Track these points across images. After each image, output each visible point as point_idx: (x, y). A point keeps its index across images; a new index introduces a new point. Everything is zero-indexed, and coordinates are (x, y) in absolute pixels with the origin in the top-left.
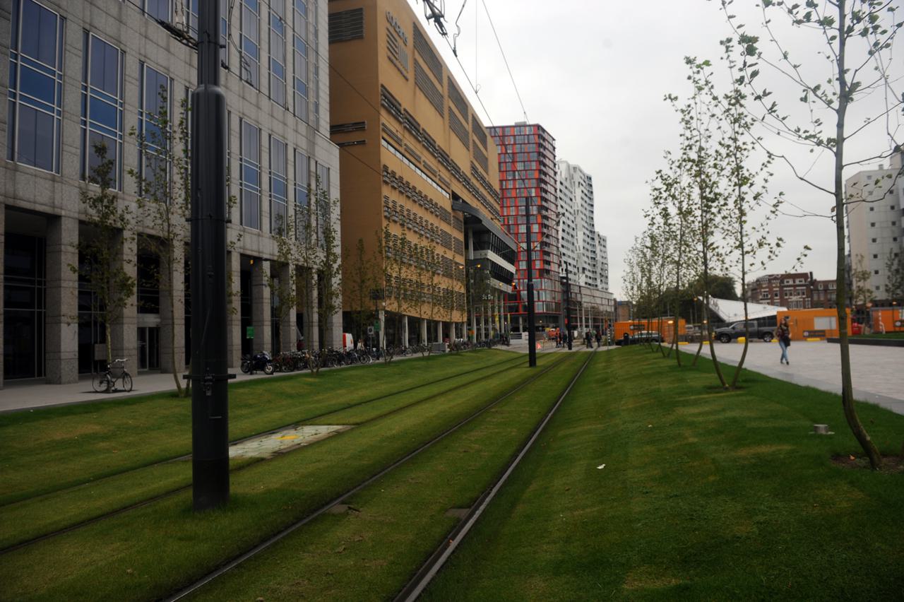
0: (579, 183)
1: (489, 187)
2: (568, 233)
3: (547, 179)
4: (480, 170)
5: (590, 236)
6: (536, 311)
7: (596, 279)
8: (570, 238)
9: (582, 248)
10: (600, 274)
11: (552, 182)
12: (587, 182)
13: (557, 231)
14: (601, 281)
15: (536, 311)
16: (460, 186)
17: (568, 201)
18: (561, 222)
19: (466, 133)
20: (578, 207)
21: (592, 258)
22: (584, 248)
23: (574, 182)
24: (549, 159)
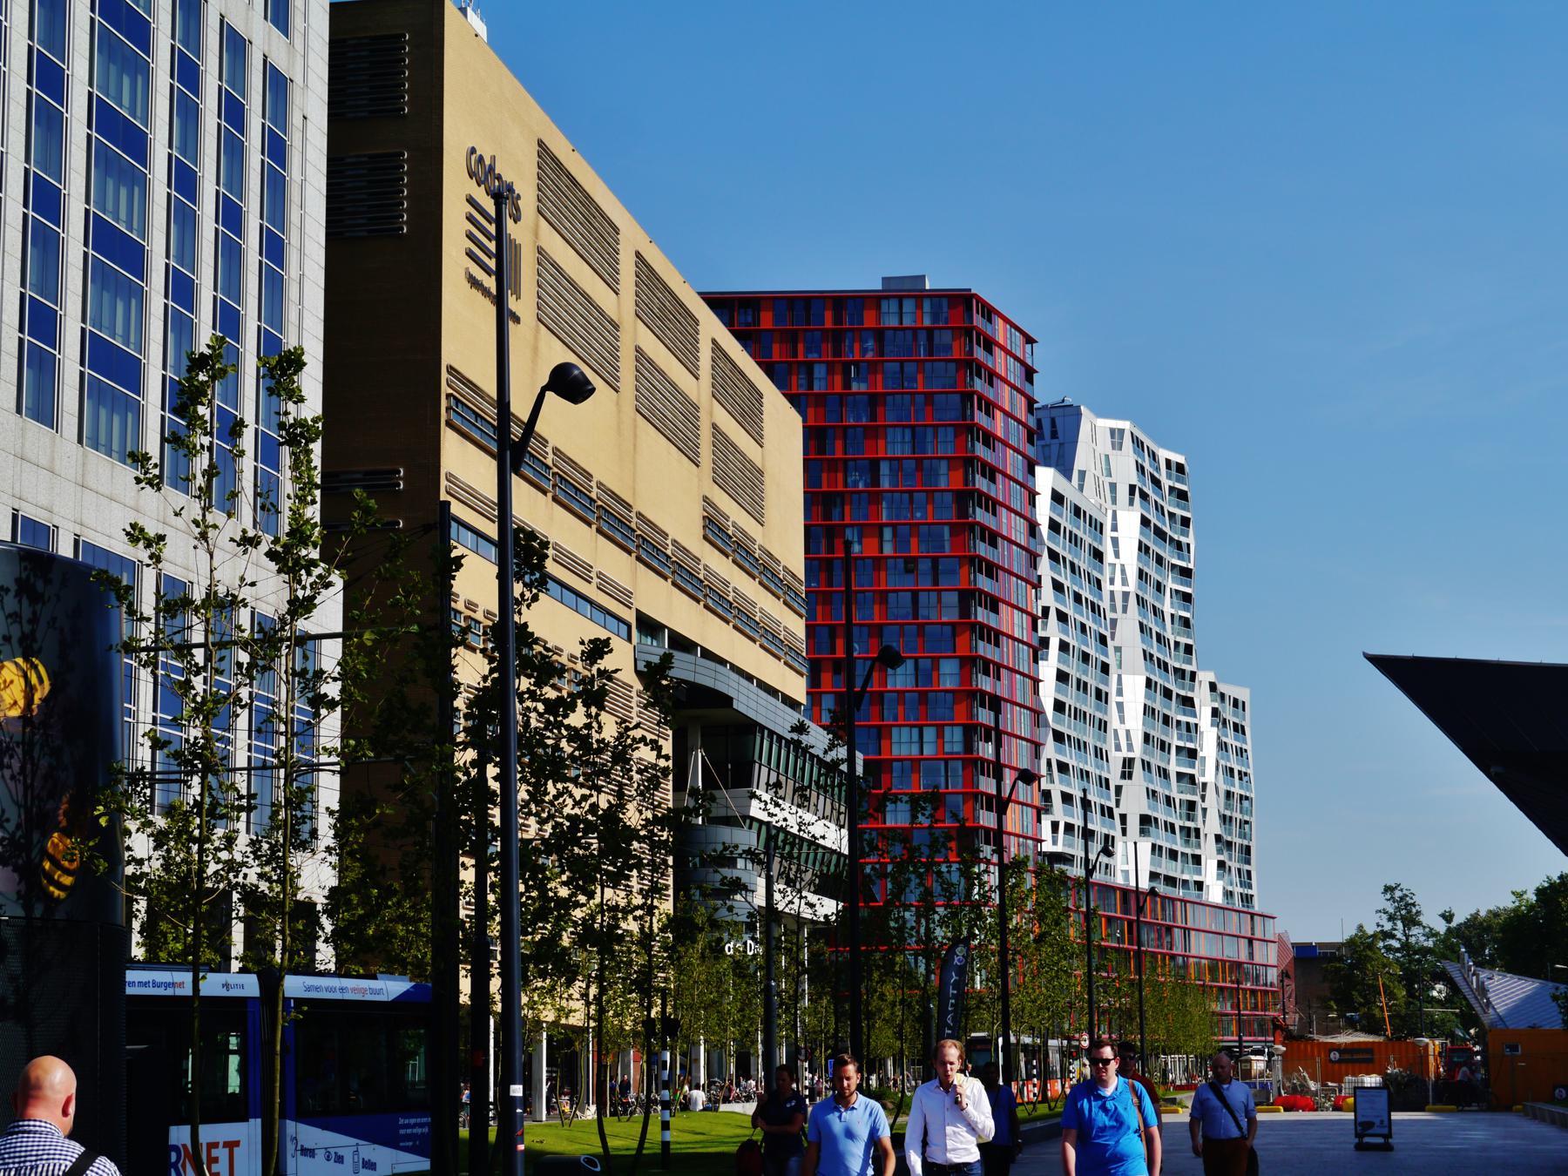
0: (1132, 488)
1: (762, 568)
2: (1082, 686)
3: (998, 490)
4: (736, 516)
5: (1175, 690)
6: (259, 1121)
7: (1197, 860)
8: (1089, 706)
9: (1138, 740)
10: (1218, 838)
11: (1017, 500)
12: (1166, 483)
13: (1036, 681)
14: (1221, 865)
15: (259, 1121)
16: (545, 501)
17: (1084, 562)
18: (1056, 799)
19: (691, 410)
20: (1125, 582)
21: (1180, 776)
22: (1147, 738)
23: (1113, 487)
24: (1008, 353)
